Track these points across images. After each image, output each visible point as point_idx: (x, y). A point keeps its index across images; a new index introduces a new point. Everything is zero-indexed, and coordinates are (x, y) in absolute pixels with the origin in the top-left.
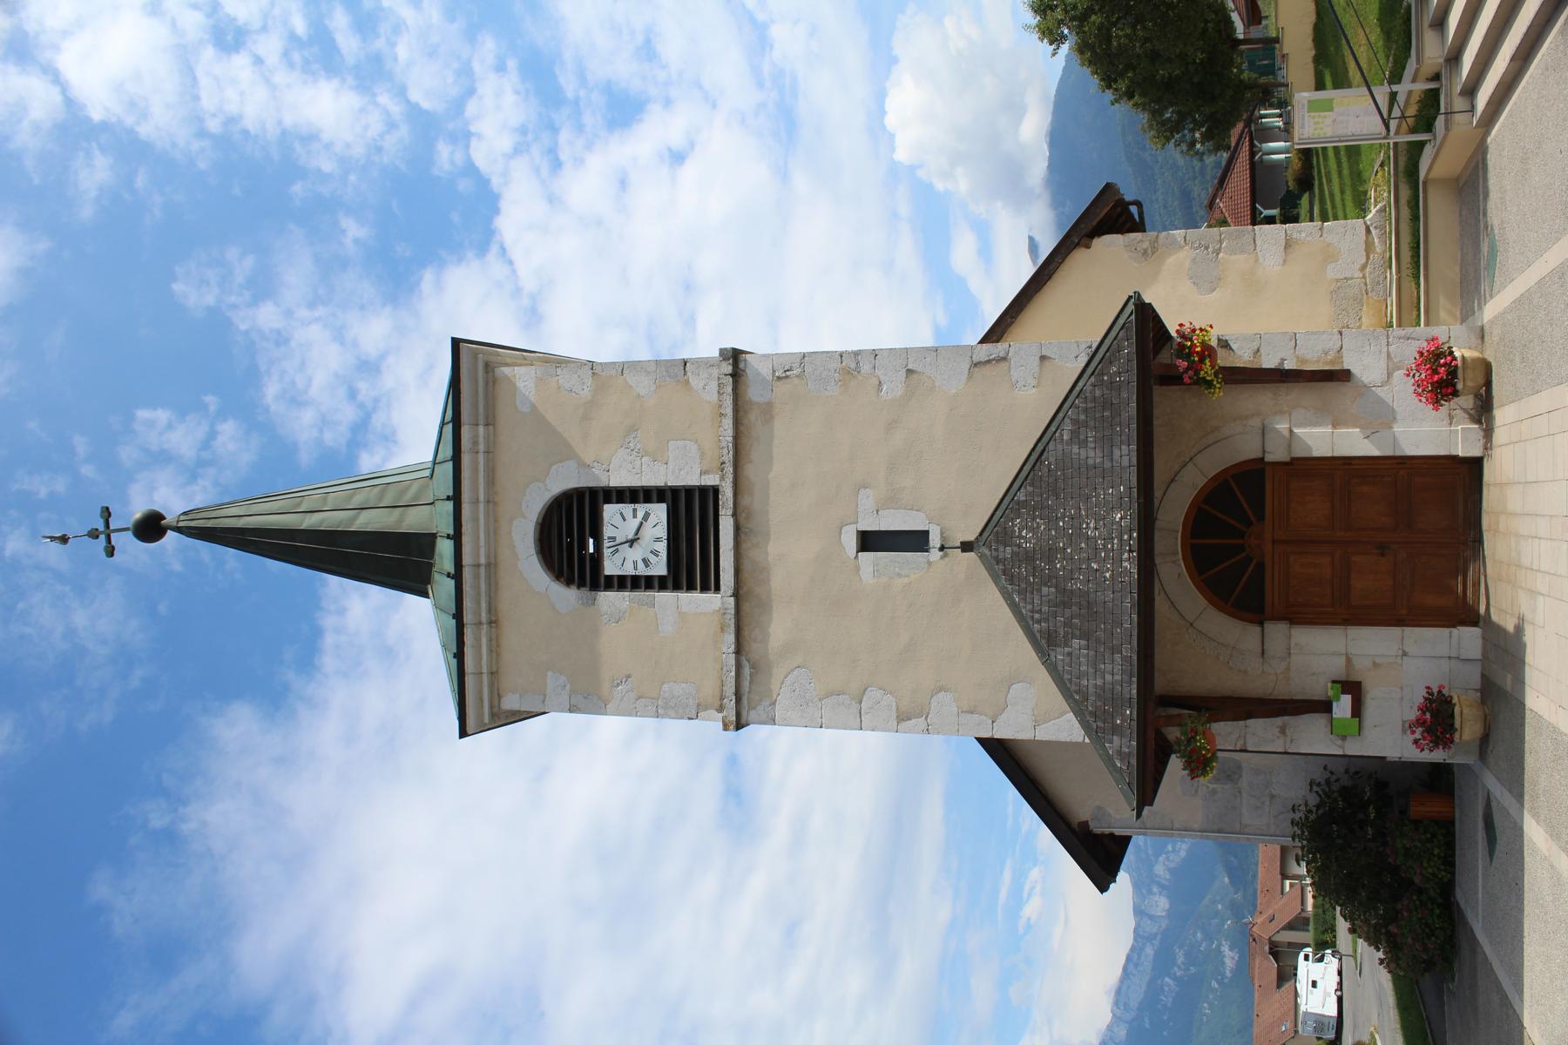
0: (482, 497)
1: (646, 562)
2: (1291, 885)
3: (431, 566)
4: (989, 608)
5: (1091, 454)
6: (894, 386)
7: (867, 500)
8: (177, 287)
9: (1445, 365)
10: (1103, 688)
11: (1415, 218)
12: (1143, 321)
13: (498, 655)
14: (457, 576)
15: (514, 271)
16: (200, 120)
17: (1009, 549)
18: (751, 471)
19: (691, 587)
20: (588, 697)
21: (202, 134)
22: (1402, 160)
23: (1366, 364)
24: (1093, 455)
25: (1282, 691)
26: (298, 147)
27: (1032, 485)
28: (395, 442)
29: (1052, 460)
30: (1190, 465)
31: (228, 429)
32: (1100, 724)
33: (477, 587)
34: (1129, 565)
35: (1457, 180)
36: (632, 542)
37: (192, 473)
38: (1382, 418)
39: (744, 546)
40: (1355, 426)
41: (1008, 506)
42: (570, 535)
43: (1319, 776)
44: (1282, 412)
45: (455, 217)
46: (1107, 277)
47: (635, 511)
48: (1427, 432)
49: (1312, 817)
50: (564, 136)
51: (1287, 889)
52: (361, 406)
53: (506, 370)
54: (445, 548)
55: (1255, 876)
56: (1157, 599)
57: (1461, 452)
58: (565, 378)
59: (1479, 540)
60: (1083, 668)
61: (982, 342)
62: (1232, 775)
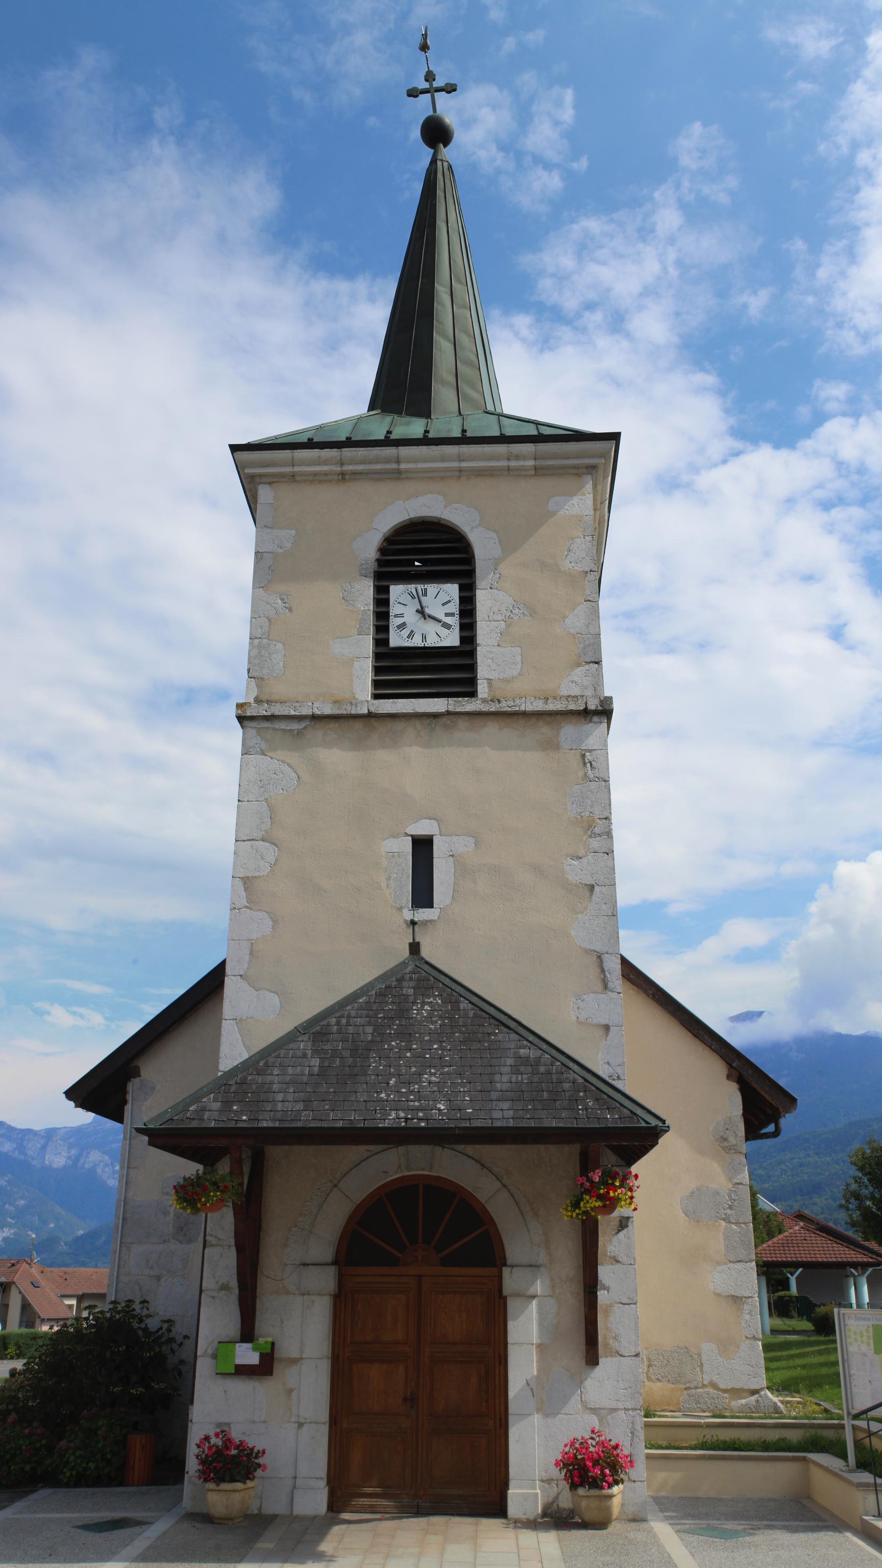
0: (464, 464)
1: (402, 626)
2: (70, 1307)
3: (399, 413)
4: (355, 970)
5: (505, 1078)
6: (577, 872)
7: (463, 845)
8: (697, 128)
9: (604, 1475)
10: (270, 1091)
11: (766, 1446)
12: (638, 1137)
13: (312, 482)
14: (388, 442)
15: (716, 465)
16: (869, 144)
17: (411, 991)
18: (491, 728)
19: (377, 670)
20: (269, 569)
21: (855, 146)
22: (829, 1434)
23: (606, 1384)
24: (504, 1080)
25: (265, 1285)
26: (842, 244)
27: (475, 1016)
28: (541, 351)
29: (500, 1037)
30: (498, 1185)
31: (554, 182)
32: (233, 1088)
33: (377, 461)
34: (392, 1118)
35: (809, 1498)
36: (421, 612)
37: (508, 146)
38: (549, 1404)
39: (418, 723)
40: (539, 1370)
41: (454, 991)
42: (428, 552)
43: (179, 1330)
44: (553, 1287)
45: (770, 405)
46: (693, 1104)
47: (452, 615)
48: (533, 1452)
49: (136, 1325)
50: (857, 512)
51: (68, 1302)
52: (578, 315)
53: (589, 486)
54: (415, 428)
55: (84, 1265)
56: (362, 1148)
57: (514, 1492)
58: (582, 545)
59: (419, 1512)
60: (290, 1070)
61: (624, 962)
62: (182, 1232)
